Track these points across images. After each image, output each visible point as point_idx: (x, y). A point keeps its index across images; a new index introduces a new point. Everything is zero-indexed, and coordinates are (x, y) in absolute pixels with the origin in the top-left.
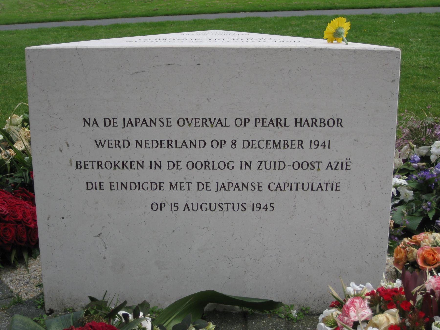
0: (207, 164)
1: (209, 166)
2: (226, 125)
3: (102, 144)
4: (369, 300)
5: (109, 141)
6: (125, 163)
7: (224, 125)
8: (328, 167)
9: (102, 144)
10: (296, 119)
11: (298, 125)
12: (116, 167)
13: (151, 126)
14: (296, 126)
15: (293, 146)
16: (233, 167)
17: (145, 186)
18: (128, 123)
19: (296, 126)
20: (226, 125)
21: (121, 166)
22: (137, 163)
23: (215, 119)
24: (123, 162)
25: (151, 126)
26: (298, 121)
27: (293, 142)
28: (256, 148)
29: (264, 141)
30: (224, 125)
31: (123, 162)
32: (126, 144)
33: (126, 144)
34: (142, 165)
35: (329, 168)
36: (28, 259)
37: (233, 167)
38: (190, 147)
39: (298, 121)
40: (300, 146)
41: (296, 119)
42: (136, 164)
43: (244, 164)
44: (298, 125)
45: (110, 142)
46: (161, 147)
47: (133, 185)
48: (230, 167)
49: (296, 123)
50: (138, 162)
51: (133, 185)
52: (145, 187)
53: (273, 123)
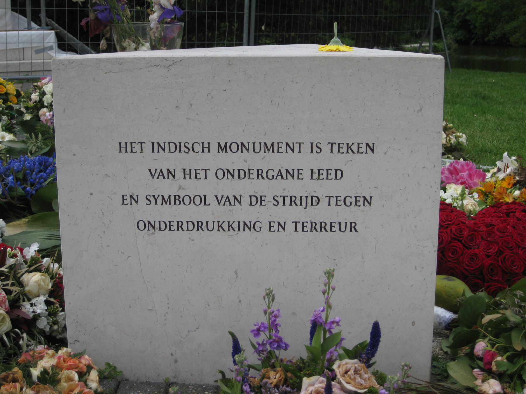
0: (200, 224)
1: (326, 227)
3: (134, 200)
6: (220, 224)
9: (134, 200)
12: (220, 228)
13: (287, 178)
14: (185, 178)
15: (358, 204)
16: (260, 228)
18: (278, 175)
19: (185, 178)
21: (226, 228)
22: (277, 224)
23: (156, 170)
24: (229, 222)
25: (287, 178)
31: (229, 222)
32: (315, 200)
33: (315, 200)
34: (283, 226)
36: (54, 348)
37: (260, 228)
38: (234, 205)
42: (276, 225)
46: (261, 204)
48: (258, 229)
50: (279, 223)
53: (163, 175)
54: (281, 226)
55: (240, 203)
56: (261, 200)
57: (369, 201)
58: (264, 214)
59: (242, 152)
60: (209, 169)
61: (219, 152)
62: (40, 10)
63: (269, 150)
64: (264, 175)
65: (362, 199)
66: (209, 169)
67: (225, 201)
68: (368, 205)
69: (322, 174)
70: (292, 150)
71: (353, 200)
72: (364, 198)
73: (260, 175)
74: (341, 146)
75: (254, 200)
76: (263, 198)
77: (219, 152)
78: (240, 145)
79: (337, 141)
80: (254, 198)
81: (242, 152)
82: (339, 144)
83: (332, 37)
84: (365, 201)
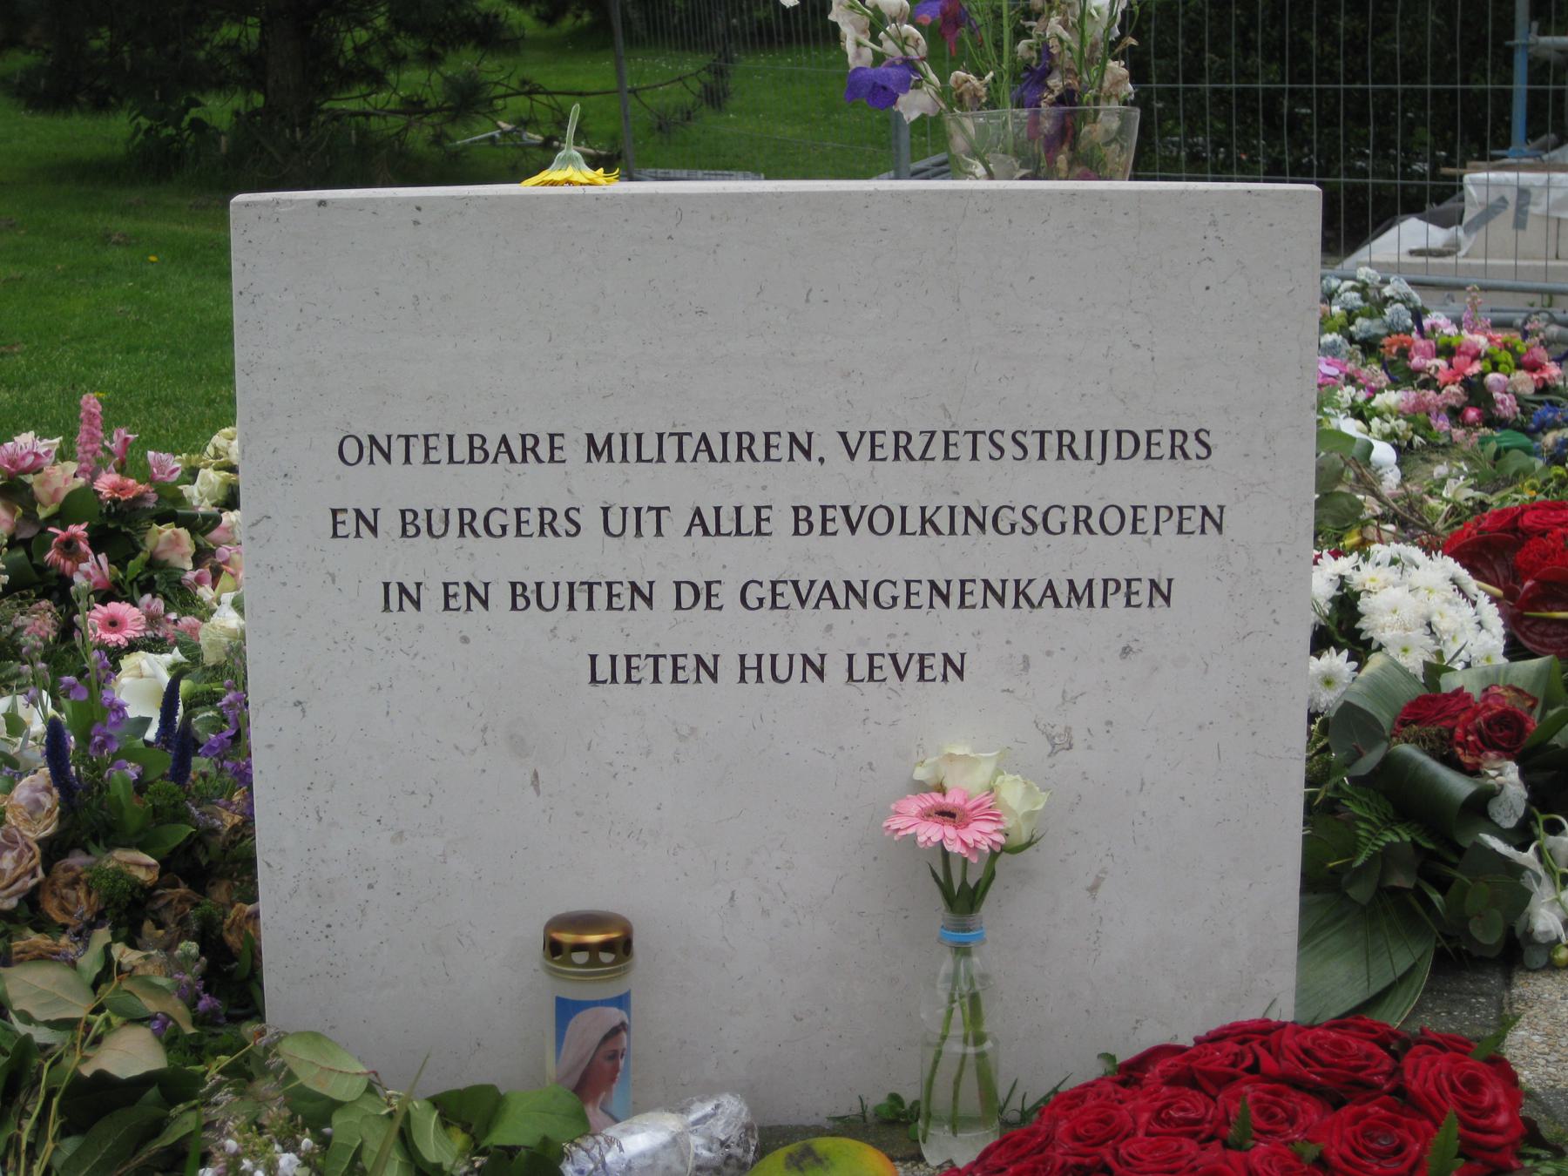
2: (718, 532)
4: (140, 498)
5: (873, 434)
6: (928, 514)
7: (712, 529)
8: (692, 524)
10: (742, 657)
11: (751, 675)
14: (743, 679)
17: (885, 594)
20: (718, 532)
26: (751, 662)
27: (774, 440)
28: (973, 607)
29: (761, 584)
30: (712, 529)
35: (698, 531)
39: (751, 662)
40: (745, 454)
41: (742, 657)
43: (955, 598)
44: (751, 675)
45: (879, 439)
47: (1128, 442)
49: (743, 668)
51: (1128, 442)
52: (885, 598)
54: (706, 668)
55: (417, 604)
56: (705, 594)
57: (482, 594)
58: (729, 632)
59: (372, 462)
60: (667, 508)
61: (589, 460)
62: (1530, 82)
63: (599, 455)
64: (479, 525)
65: (463, 590)
66: (667, 508)
67: (820, 598)
68: (480, 607)
69: (768, 519)
70: (387, 457)
71: (901, 591)
72: (987, 583)
73: (467, 523)
74: (432, 442)
75: (687, 595)
76: (715, 589)
77: (589, 460)
78: (366, 443)
79: (421, 432)
80: (689, 588)
81: (372, 462)
82: (426, 437)
83: (1505, 143)
84: (1000, 592)
